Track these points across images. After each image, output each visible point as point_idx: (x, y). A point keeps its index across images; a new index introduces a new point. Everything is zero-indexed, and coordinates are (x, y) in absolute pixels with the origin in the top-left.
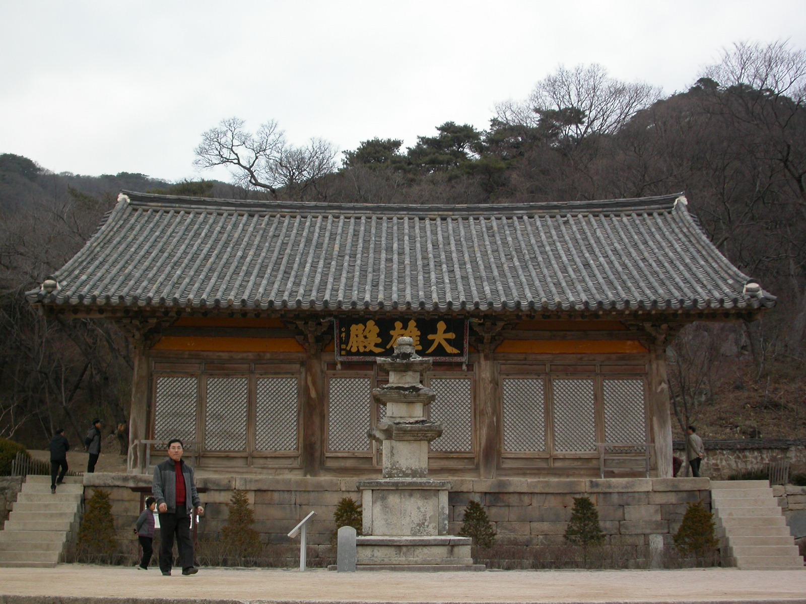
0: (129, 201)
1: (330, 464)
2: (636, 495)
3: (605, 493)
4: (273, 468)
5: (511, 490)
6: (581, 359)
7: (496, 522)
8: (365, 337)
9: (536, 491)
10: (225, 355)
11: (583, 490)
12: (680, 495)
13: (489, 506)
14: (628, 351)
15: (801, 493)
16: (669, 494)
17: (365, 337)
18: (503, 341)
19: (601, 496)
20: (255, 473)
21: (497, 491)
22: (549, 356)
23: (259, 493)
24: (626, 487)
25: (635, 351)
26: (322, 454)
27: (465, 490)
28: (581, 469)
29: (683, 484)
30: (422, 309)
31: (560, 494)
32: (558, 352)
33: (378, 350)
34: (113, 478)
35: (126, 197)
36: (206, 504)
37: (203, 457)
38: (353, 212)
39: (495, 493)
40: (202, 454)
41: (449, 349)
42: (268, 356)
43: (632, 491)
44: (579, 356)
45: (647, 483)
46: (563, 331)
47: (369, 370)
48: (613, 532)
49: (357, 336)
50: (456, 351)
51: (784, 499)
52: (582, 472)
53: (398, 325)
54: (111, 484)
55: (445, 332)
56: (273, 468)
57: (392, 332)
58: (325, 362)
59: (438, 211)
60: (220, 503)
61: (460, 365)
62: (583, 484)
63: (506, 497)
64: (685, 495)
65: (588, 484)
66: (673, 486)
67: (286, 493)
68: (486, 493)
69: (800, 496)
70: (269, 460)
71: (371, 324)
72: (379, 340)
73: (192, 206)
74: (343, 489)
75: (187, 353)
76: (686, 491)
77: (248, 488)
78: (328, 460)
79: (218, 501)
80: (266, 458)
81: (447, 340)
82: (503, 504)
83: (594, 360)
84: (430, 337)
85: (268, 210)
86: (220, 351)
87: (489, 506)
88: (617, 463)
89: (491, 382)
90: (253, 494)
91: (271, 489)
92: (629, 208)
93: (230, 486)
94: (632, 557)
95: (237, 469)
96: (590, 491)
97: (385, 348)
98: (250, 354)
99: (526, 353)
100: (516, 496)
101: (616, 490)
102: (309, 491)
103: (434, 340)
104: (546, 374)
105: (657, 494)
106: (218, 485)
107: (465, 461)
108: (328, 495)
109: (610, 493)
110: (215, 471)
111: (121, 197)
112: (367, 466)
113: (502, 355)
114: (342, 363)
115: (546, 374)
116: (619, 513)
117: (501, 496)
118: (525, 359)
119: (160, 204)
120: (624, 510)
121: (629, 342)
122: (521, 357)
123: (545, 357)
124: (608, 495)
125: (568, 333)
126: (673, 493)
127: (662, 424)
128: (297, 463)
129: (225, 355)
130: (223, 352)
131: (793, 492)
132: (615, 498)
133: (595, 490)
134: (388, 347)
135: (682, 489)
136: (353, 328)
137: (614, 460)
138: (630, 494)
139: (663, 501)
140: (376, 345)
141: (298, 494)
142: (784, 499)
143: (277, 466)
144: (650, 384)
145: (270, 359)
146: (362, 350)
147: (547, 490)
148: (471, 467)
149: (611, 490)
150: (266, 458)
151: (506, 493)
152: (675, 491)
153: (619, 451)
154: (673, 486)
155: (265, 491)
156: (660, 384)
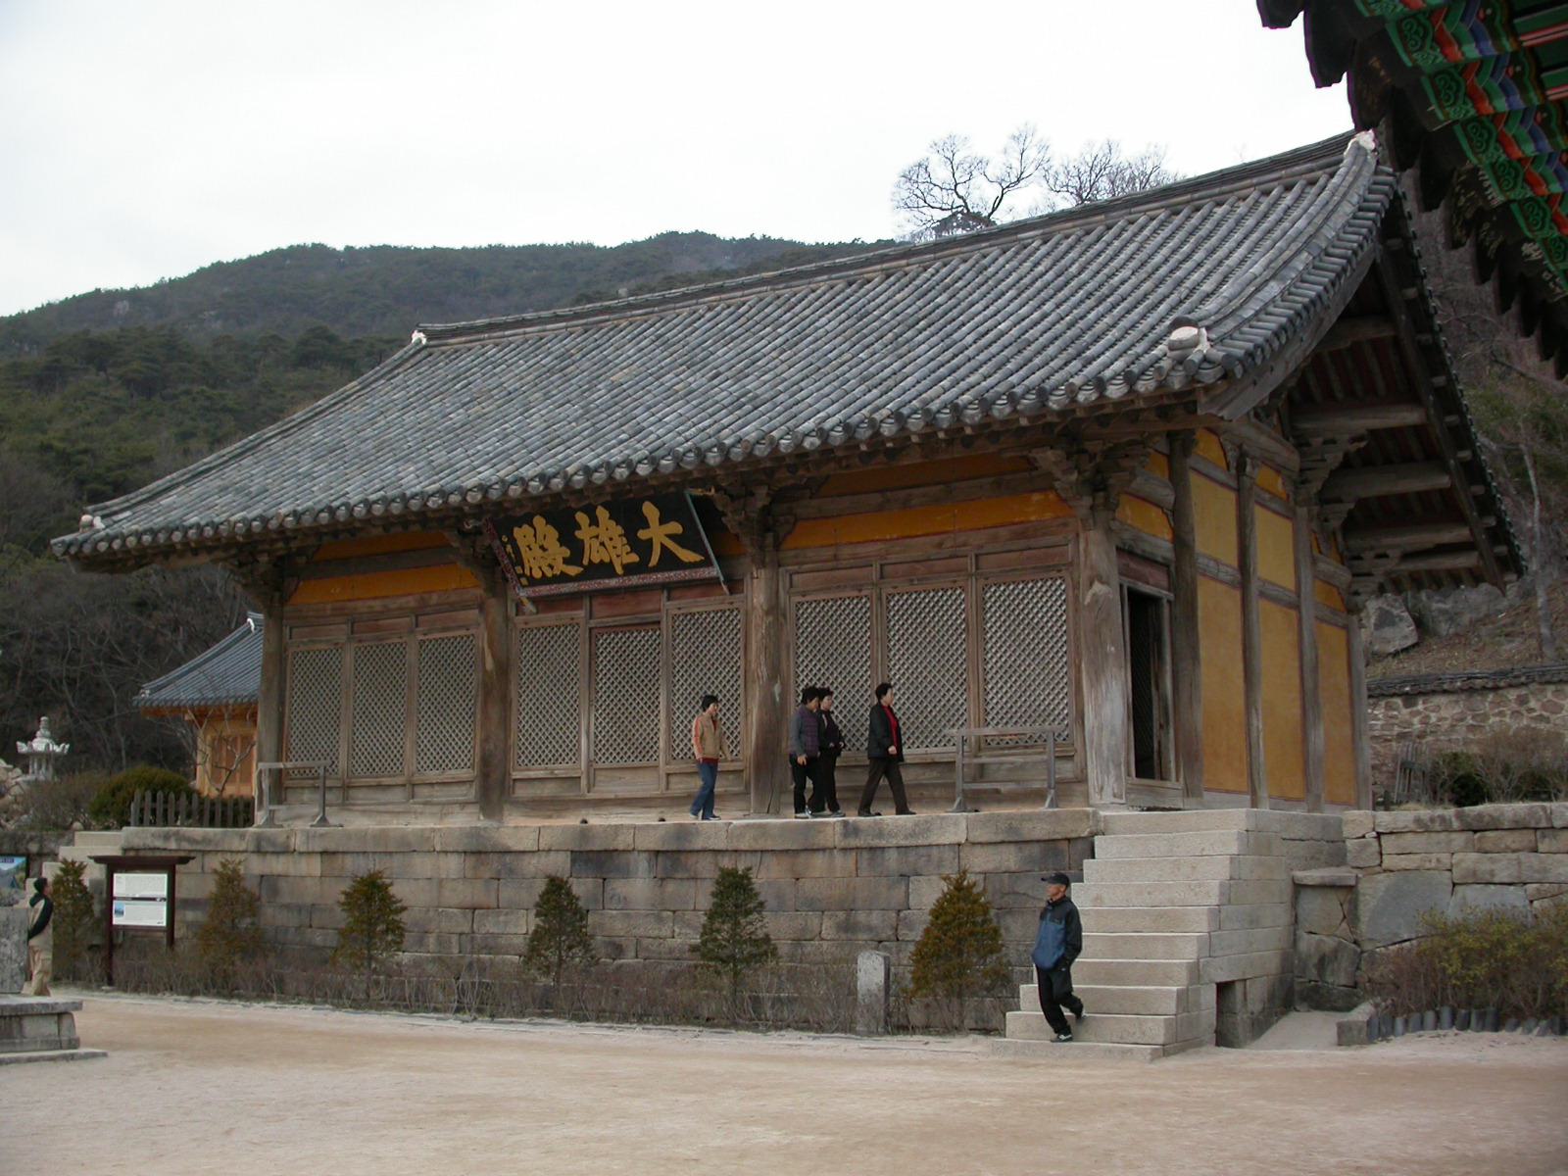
0: (424, 341)
1: (522, 792)
2: (935, 851)
3: (872, 849)
4: (438, 804)
5: (698, 844)
6: (940, 545)
7: (674, 912)
8: (542, 548)
9: (743, 846)
10: (377, 605)
11: (830, 844)
12: (1027, 850)
13: (662, 879)
14: (1033, 518)
15: (1413, 827)
16: (1003, 848)
17: (542, 548)
18: (794, 524)
19: (865, 855)
20: (415, 813)
21: (674, 848)
22: (880, 546)
23: (326, 857)
24: (913, 835)
25: (1048, 515)
26: (506, 774)
27: (621, 847)
28: (935, 786)
29: (1030, 825)
30: (547, 487)
31: (787, 851)
32: (895, 536)
33: (573, 570)
34: (153, 835)
35: (422, 335)
36: (262, 876)
37: (348, 787)
38: (739, 293)
39: (673, 851)
40: (347, 781)
41: (687, 555)
42: (434, 599)
43: (926, 843)
44: (937, 539)
45: (956, 824)
46: (903, 488)
47: (575, 609)
48: (883, 936)
49: (611, 539)
50: (698, 558)
51: (1368, 845)
52: (937, 793)
53: (582, 518)
54: (152, 846)
55: (662, 521)
56: (438, 804)
57: (578, 534)
58: (513, 600)
59: (883, 262)
60: (279, 876)
61: (713, 583)
62: (829, 830)
63: (693, 858)
64: (1036, 849)
65: (839, 829)
66: (1010, 829)
67: (361, 857)
68: (657, 852)
69: (1409, 835)
70: (437, 788)
71: (539, 521)
72: (567, 553)
73: (507, 333)
74: (438, 848)
75: (329, 606)
76: (1038, 841)
77: (310, 850)
78: (518, 784)
79: (275, 872)
80: (432, 784)
81: (671, 537)
82: (686, 875)
83: (965, 545)
84: (643, 534)
85: (612, 317)
86: (369, 599)
87: (662, 879)
88: (1009, 770)
89: (767, 613)
90: (318, 858)
91: (341, 850)
92: (1247, 182)
93: (288, 846)
94: (826, 1010)
95: (390, 808)
96: (843, 845)
97: (581, 565)
98: (410, 598)
99: (836, 545)
100: (710, 858)
101: (894, 842)
102: (391, 853)
103: (662, 545)
104: (873, 584)
105: (978, 850)
106: (273, 844)
107: (731, 777)
108: (417, 859)
109: (883, 848)
110: (364, 812)
111: (416, 336)
112: (570, 795)
113: (792, 553)
114: (534, 600)
115: (873, 584)
116: (898, 893)
117: (683, 857)
118: (836, 558)
119: (463, 339)
120: (908, 886)
121: (1036, 497)
122: (828, 553)
123: (871, 549)
124: (878, 852)
125: (915, 491)
126: (1012, 848)
127: (1097, 675)
128: (471, 793)
129: (377, 605)
130: (375, 598)
131: (1391, 827)
132: (892, 859)
133: (853, 842)
134: (585, 562)
135: (1027, 837)
136: (517, 532)
137: (1002, 764)
138: (922, 851)
139: (990, 867)
140: (566, 561)
141: (377, 857)
142: (1368, 845)
143: (444, 799)
144: (1076, 586)
145: (437, 605)
146: (549, 574)
147: (761, 845)
148: (736, 789)
149: (883, 843)
150: (432, 784)
151: (690, 851)
152: (1016, 842)
153: (1011, 744)
154: (1010, 829)
155: (334, 853)
156: (1091, 585)
